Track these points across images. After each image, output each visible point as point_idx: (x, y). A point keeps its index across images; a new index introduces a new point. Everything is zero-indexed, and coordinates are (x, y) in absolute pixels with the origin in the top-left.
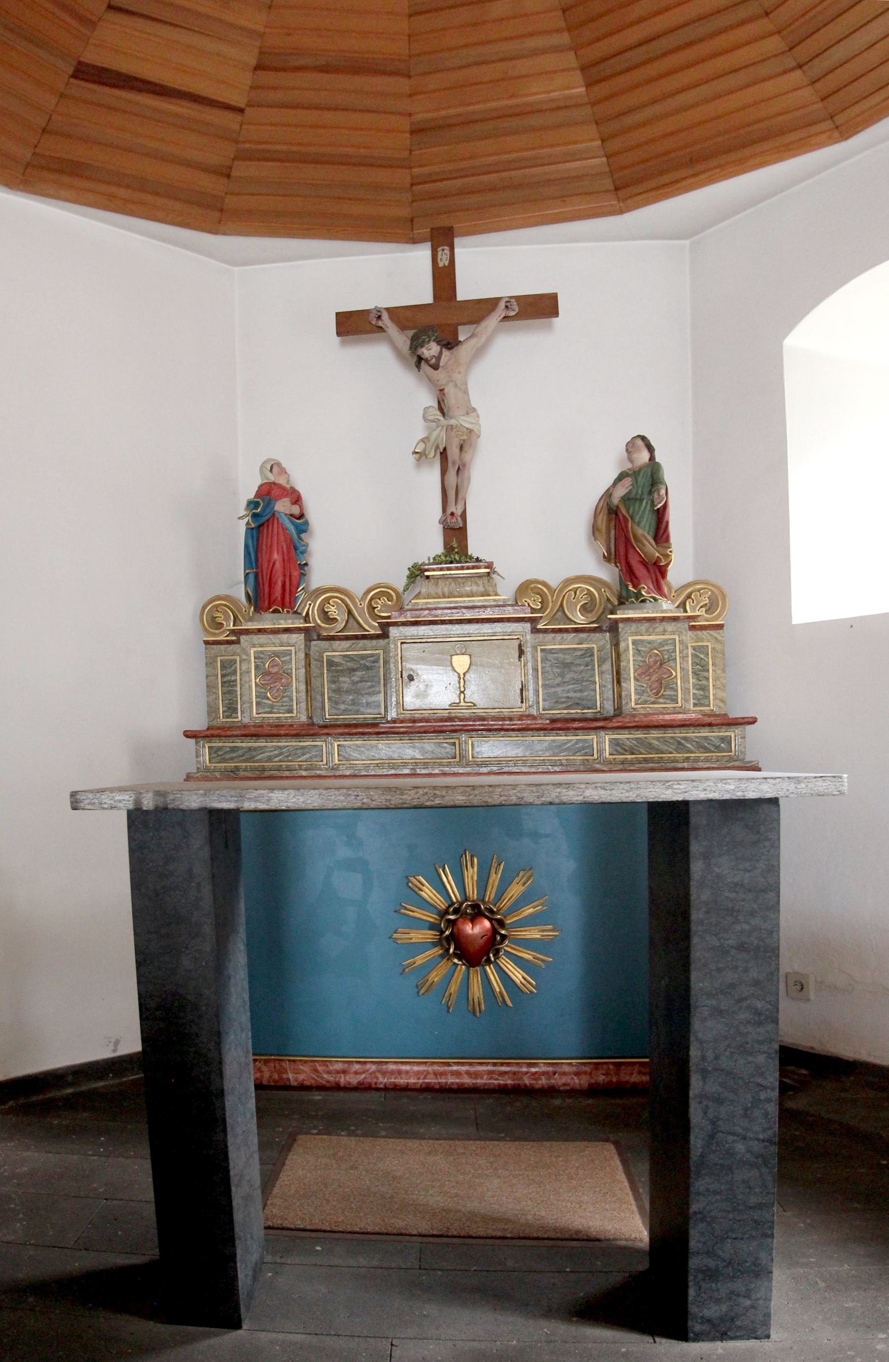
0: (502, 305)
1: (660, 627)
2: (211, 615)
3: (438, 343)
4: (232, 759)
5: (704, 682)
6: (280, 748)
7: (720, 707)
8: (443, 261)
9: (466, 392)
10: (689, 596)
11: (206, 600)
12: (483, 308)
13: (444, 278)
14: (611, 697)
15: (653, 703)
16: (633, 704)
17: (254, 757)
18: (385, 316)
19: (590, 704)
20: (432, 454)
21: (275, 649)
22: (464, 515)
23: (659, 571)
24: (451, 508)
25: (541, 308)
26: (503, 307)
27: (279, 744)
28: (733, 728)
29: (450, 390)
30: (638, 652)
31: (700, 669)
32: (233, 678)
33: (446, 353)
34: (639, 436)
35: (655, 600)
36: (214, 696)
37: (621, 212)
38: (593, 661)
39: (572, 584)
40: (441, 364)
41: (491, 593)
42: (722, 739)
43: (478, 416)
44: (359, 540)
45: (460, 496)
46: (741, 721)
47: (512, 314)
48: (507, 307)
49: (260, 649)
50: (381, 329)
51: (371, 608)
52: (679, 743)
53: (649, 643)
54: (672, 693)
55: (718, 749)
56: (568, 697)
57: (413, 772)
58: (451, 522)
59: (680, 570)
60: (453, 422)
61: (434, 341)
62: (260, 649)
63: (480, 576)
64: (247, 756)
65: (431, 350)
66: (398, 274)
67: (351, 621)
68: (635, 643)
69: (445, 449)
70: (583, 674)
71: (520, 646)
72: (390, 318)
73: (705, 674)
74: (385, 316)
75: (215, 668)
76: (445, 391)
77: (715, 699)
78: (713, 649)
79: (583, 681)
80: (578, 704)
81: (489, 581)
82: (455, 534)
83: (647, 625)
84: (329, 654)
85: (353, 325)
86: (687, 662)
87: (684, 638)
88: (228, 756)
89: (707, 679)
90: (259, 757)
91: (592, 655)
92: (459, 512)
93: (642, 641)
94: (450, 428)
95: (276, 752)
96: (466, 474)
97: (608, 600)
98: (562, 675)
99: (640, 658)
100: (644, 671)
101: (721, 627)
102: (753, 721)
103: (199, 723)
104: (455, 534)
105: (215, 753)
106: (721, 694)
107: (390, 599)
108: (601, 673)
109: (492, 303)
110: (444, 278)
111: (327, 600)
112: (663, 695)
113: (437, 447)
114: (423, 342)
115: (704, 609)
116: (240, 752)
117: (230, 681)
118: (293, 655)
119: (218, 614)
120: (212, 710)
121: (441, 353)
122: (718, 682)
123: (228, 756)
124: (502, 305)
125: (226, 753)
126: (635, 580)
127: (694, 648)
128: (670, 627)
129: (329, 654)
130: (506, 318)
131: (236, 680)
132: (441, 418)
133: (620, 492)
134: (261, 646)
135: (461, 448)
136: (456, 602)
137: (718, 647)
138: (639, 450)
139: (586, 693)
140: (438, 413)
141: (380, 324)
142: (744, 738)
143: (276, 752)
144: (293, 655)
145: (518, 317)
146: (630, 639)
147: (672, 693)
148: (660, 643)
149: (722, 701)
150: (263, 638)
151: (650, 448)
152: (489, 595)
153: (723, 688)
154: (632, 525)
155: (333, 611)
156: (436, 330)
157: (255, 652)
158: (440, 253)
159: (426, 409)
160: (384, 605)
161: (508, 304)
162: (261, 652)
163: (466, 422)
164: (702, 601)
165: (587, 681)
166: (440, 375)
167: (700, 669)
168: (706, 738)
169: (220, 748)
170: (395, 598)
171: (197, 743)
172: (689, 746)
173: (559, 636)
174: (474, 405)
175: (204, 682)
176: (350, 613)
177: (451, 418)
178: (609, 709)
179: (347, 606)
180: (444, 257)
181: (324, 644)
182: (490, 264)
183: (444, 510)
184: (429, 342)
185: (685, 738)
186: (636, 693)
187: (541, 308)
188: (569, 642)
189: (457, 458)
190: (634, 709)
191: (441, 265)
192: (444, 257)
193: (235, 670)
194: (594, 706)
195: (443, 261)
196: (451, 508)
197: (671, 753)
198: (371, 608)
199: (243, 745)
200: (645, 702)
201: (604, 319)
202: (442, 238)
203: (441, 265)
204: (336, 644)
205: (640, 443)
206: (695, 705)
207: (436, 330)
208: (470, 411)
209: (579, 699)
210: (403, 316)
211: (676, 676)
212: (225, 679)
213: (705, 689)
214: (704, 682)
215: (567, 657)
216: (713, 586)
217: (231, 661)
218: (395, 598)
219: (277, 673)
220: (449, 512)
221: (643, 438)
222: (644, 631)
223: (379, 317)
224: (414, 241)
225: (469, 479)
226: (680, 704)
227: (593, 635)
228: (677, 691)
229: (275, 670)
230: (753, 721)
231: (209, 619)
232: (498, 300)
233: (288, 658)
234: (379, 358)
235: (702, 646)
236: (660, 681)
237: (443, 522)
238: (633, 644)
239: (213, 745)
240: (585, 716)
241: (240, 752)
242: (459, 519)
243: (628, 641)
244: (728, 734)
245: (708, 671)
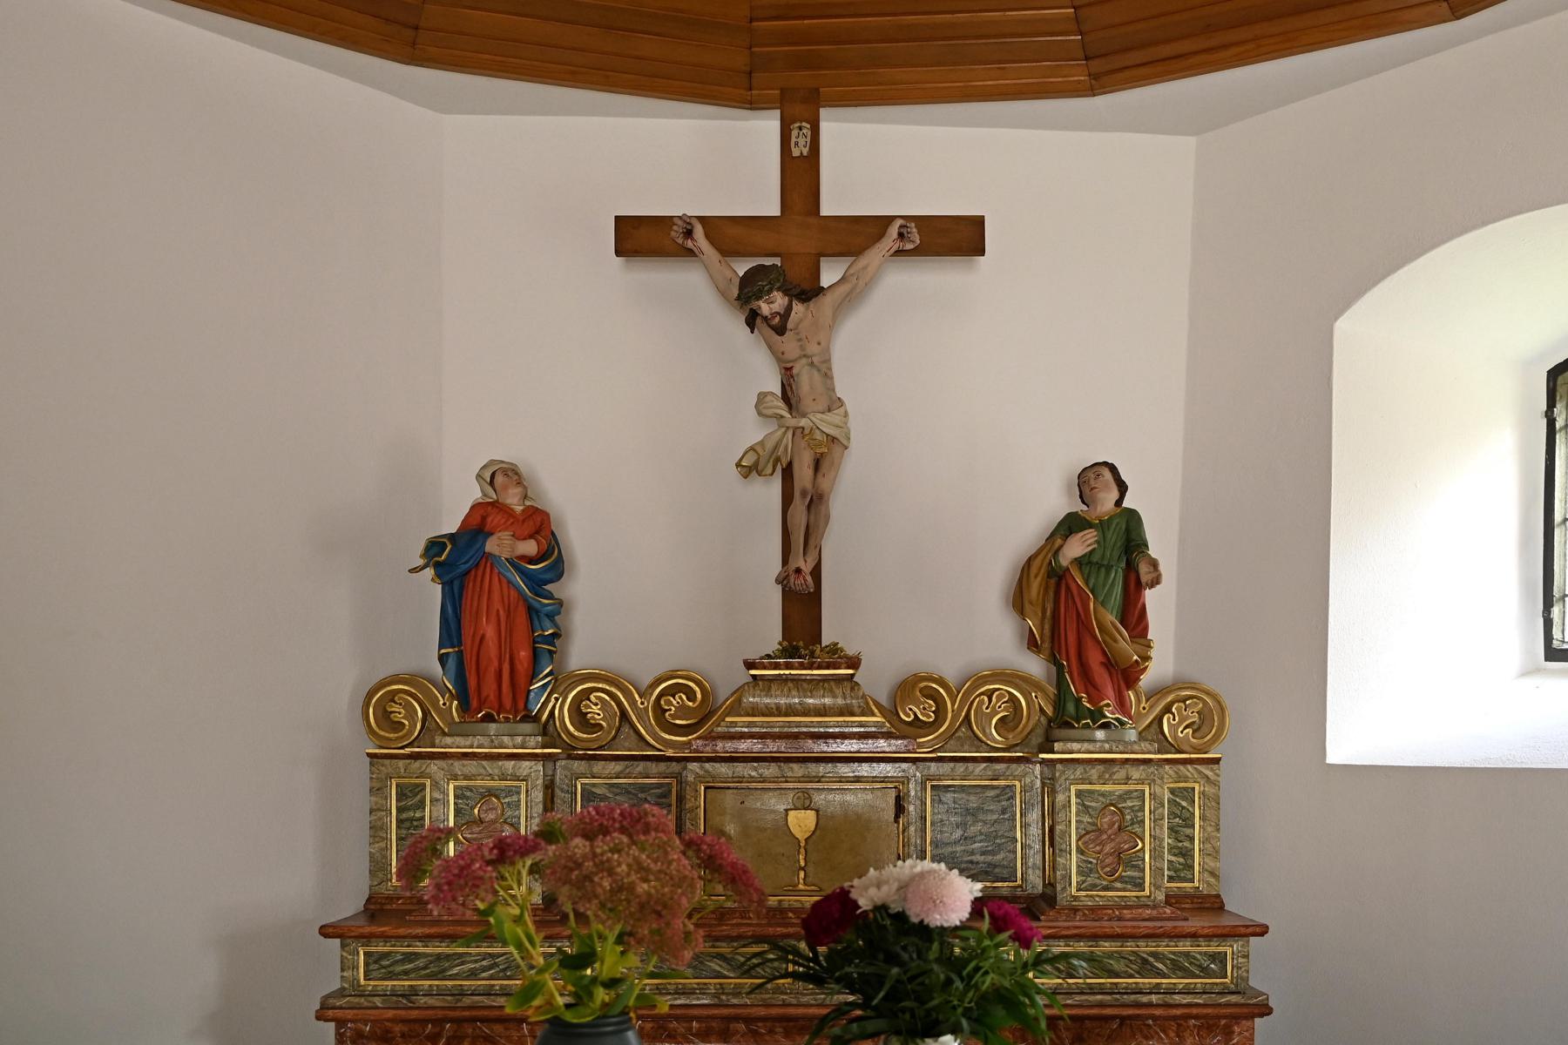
0: (893, 231)
1: (1121, 774)
2: (382, 706)
3: (786, 292)
4: (406, 973)
5: (1187, 844)
6: (491, 956)
7: (1209, 884)
8: (800, 148)
9: (827, 376)
10: (1168, 709)
11: (375, 681)
12: (861, 234)
13: (800, 173)
14: (1039, 862)
15: (1106, 889)
16: (1074, 890)
17: (444, 970)
18: (699, 231)
19: (1005, 873)
20: (769, 470)
21: (492, 783)
22: (816, 573)
23: (1128, 676)
24: (799, 561)
25: (959, 238)
26: (895, 235)
27: (490, 950)
28: (1230, 941)
29: (800, 368)
30: (1084, 809)
31: (1181, 823)
32: (418, 815)
33: (798, 308)
34: (1105, 464)
35: (1122, 723)
36: (382, 845)
37: (1092, 91)
38: (1013, 806)
39: (986, 683)
40: (790, 325)
41: (856, 710)
42: (1213, 957)
43: (846, 415)
44: (653, 594)
45: (812, 542)
46: (1243, 930)
47: (909, 246)
48: (901, 235)
49: (465, 783)
50: (690, 253)
51: (659, 711)
52: (1145, 961)
53: (1103, 795)
54: (1136, 874)
55: (1206, 972)
56: (971, 862)
57: (716, 1001)
58: (796, 583)
59: (1160, 666)
60: (803, 422)
61: (779, 289)
62: (465, 783)
63: (839, 680)
64: (433, 968)
65: (772, 304)
66: (717, 158)
67: (626, 729)
68: (1079, 794)
69: (790, 464)
70: (997, 826)
71: (898, 798)
72: (707, 236)
73: (1188, 831)
74: (699, 231)
75: (387, 798)
76: (795, 371)
77: (1203, 870)
78: (1203, 793)
79: (996, 837)
80: (987, 873)
81: (852, 689)
82: (802, 604)
83: (1101, 768)
84: (586, 781)
85: (640, 238)
86: (1161, 828)
87: (1158, 790)
88: (399, 968)
89: (1192, 839)
90: (455, 971)
91: (1013, 797)
92: (807, 568)
93: (1091, 792)
94: (798, 431)
95: (484, 963)
96: (823, 508)
97: (1041, 709)
98: (963, 825)
99: (1087, 819)
100: (1090, 834)
101: (1217, 761)
102: (1263, 931)
103: (349, 905)
104: (802, 604)
105: (375, 962)
106: (1211, 864)
107: (691, 695)
108: (1025, 826)
109: (881, 224)
110: (800, 173)
111: (586, 694)
112: (1121, 877)
113: (778, 460)
114: (760, 291)
115: (1189, 731)
116: (421, 963)
117: (412, 820)
118: (523, 796)
119: (396, 708)
120: (378, 866)
121: (789, 309)
122: (1208, 846)
123: (399, 968)
124: (893, 231)
125: (397, 962)
126: (1091, 689)
127: (1172, 791)
128: (1136, 773)
129: (586, 781)
130: (899, 253)
131: (423, 818)
132: (788, 415)
133: (1076, 547)
134: (466, 778)
135: (817, 465)
136: (799, 724)
137: (1209, 789)
138: (1106, 486)
139: (999, 857)
140: (781, 404)
141: (689, 244)
142: (1247, 956)
143: (484, 963)
144: (523, 796)
145: (917, 252)
146: (1073, 788)
147: (1136, 874)
148: (1120, 796)
149: (1213, 874)
150: (471, 766)
151: (1122, 488)
152: (853, 715)
153: (1215, 854)
154: (1086, 582)
155: (595, 711)
156: (784, 267)
157: (456, 788)
158: (794, 133)
159: (762, 397)
160: (682, 707)
161: (904, 231)
162: (468, 788)
163: (826, 423)
164: (1187, 717)
165: (1003, 836)
166: (788, 344)
167: (1181, 823)
168: (1187, 955)
169: (386, 955)
170: (699, 696)
171: (343, 946)
172: (1160, 966)
173: (961, 767)
174: (840, 392)
175: (366, 819)
176: (624, 715)
177: (804, 415)
178: (1036, 883)
179: (619, 704)
180: (802, 141)
181: (578, 766)
182: (881, 157)
183: (785, 562)
184: (770, 291)
185: (1155, 955)
186: (1078, 873)
187: (959, 238)
188: (978, 776)
189: (809, 486)
190: (1076, 898)
191: (796, 152)
192: (802, 141)
193: (423, 802)
194: (1012, 877)
195: (800, 148)
196: (799, 561)
197: (1131, 976)
198: (659, 711)
199: (428, 950)
200: (1093, 887)
201: (1055, 279)
202: (800, 114)
203: (796, 152)
204: (598, 767)
205: (1107, 474)
206: (1171, 879)
207: (784, 267)
208: (835, 404)
209: (990, 864)
210: (728, 234)
211: (1143, 849)
212: (404, 816)
213: (1187, 854)
214: (1187, 844)
215: (972, 798)
216: (1208, 693)
217: (417, 785)
218: (699, 696)
219: (494, 822)
220: (792, 566)
221: (1112, 468)
222: (1095, 777)
223: (689, 233)
224: (753, 104)
225: (828, 517)
226: (1147, 892)
227: (1014, 766)
228: (1143, 870)
229: (491, 816)
230: (1263, 931)
231: (380, 714)
232: (889, 220)
233: (515, 798)
234: (693, 288)
235: (1185, 789)
236: (1118, 854)
237: (782, 580)
238: (1077, 796)
239: (373, 949)
240: (996, 892)
241: (421, 963)
242: (809, 578)
243: (1070, 796)
244: (1221, 949)
245: (1193, 826)
